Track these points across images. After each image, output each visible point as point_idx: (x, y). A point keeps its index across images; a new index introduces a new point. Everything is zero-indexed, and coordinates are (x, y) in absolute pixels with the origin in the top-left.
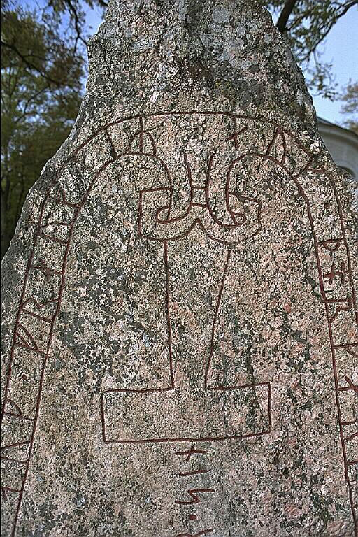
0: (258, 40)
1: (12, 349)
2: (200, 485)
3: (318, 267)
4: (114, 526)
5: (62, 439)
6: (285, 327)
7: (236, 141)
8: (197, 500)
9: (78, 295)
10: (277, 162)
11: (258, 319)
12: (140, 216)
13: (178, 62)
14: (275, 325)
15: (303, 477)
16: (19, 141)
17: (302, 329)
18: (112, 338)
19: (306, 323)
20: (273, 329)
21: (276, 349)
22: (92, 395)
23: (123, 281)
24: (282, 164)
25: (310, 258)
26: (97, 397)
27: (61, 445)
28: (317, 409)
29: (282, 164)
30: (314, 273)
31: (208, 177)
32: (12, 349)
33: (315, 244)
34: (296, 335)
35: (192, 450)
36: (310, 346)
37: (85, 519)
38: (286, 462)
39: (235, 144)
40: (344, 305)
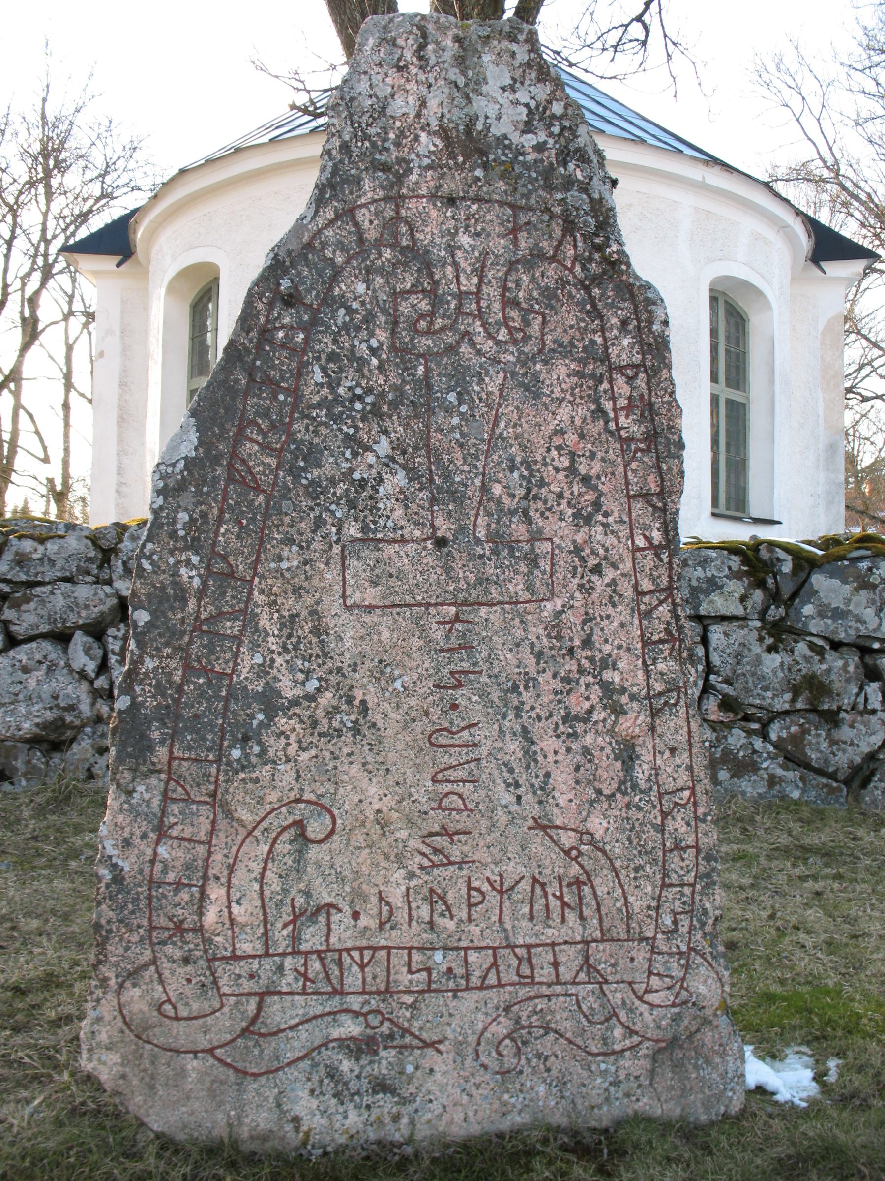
0: (545, 109)
1: (227, 486)
2: (465, 665)
3: (613, 399)
4: (353, 717)
5: (289, 604)
6: (572, 470)
7: (516, 238)
8: (460, 685)
9: (314, 419)
10: (566, 268)
11: (539, 458)
12: (396, 323)
13: (443, 132)
14: (560, 466)
15: (591, 660)
16: (630, 332)
17: (593, 473)
18: (357, 476)
19: (597, 467)
20: (557, 470)
21: (560, 496)
22: (331, 547)
23: (373, 404)
24: (571, 270)
25: (605, 385)
26: (336, 549)
27: (286, 613)
28: (610, 574)
29: (571, 270)
30: (608, 405)
31: (481, 281)
32: (227, 486)
33: (610, 369)
34: (586, 480)
35: (457, 619)
36: (601, 494)
37: (317, 707)
38: (571, 639)
39: (515, 242)
40: (642, 446)
